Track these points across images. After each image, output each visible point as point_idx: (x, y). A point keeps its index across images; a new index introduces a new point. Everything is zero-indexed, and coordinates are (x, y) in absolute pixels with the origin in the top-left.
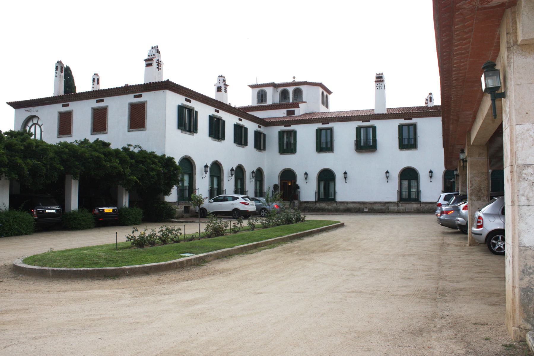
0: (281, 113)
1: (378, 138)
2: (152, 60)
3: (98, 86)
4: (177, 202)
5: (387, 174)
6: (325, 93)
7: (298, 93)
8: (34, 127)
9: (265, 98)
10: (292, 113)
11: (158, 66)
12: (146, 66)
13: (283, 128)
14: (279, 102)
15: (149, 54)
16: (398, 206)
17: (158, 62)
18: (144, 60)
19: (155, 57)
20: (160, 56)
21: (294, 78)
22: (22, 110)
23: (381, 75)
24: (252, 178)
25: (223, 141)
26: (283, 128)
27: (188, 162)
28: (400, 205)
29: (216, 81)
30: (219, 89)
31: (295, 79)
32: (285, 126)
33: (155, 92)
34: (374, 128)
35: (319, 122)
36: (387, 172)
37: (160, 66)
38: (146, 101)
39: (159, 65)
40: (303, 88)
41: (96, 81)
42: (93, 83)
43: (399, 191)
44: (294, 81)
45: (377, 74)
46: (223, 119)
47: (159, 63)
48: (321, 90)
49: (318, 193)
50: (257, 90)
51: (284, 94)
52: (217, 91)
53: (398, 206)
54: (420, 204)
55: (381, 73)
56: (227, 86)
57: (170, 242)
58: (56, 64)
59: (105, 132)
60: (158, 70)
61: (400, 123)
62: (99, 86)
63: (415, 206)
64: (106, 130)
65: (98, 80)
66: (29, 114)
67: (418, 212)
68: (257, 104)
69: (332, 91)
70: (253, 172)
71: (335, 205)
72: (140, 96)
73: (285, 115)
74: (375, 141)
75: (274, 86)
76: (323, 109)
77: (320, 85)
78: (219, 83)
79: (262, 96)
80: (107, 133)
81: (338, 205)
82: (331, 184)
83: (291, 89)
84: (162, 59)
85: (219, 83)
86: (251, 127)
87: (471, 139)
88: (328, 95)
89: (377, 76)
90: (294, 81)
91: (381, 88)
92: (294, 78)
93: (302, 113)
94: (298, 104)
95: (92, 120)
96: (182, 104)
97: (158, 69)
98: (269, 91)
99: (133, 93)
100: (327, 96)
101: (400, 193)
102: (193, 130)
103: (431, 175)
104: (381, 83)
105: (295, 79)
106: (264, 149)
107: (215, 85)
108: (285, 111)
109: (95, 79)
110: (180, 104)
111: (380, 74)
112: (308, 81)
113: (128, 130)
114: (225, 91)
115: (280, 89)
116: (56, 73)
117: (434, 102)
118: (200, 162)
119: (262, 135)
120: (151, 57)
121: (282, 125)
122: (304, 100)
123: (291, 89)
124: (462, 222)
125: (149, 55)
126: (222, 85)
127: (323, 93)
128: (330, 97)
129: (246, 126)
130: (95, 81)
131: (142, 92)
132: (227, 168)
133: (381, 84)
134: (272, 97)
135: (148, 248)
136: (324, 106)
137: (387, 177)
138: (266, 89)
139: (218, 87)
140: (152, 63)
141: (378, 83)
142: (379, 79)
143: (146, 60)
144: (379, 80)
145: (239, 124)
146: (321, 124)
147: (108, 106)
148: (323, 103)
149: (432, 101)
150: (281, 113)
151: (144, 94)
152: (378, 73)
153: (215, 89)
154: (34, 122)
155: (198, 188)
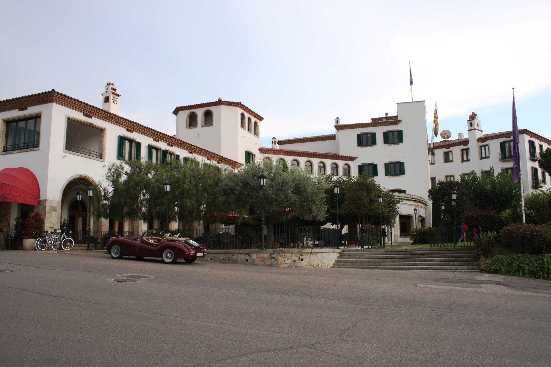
6: (253, 119)
9: (380, 138)
29: (103, 90)
30: (107, 100)
32: (464, 146)
35: (461, 145)
48: (240, 111)
54: (520, 137)
58: (106, 86)
61: (247, 150)
78: (107, 92)
85: (107, 92)
87: (11, 222)
88: (258, 121)
94: (92, 117)
95: (16, 117)
100: (256, 123)
124: (168, 182)
127: (243, 115)
128: (261, 124)
135: (65, 157)
136: (245, 130)
139: (106, 97)
142: (411, 83)
153: (102, 99)
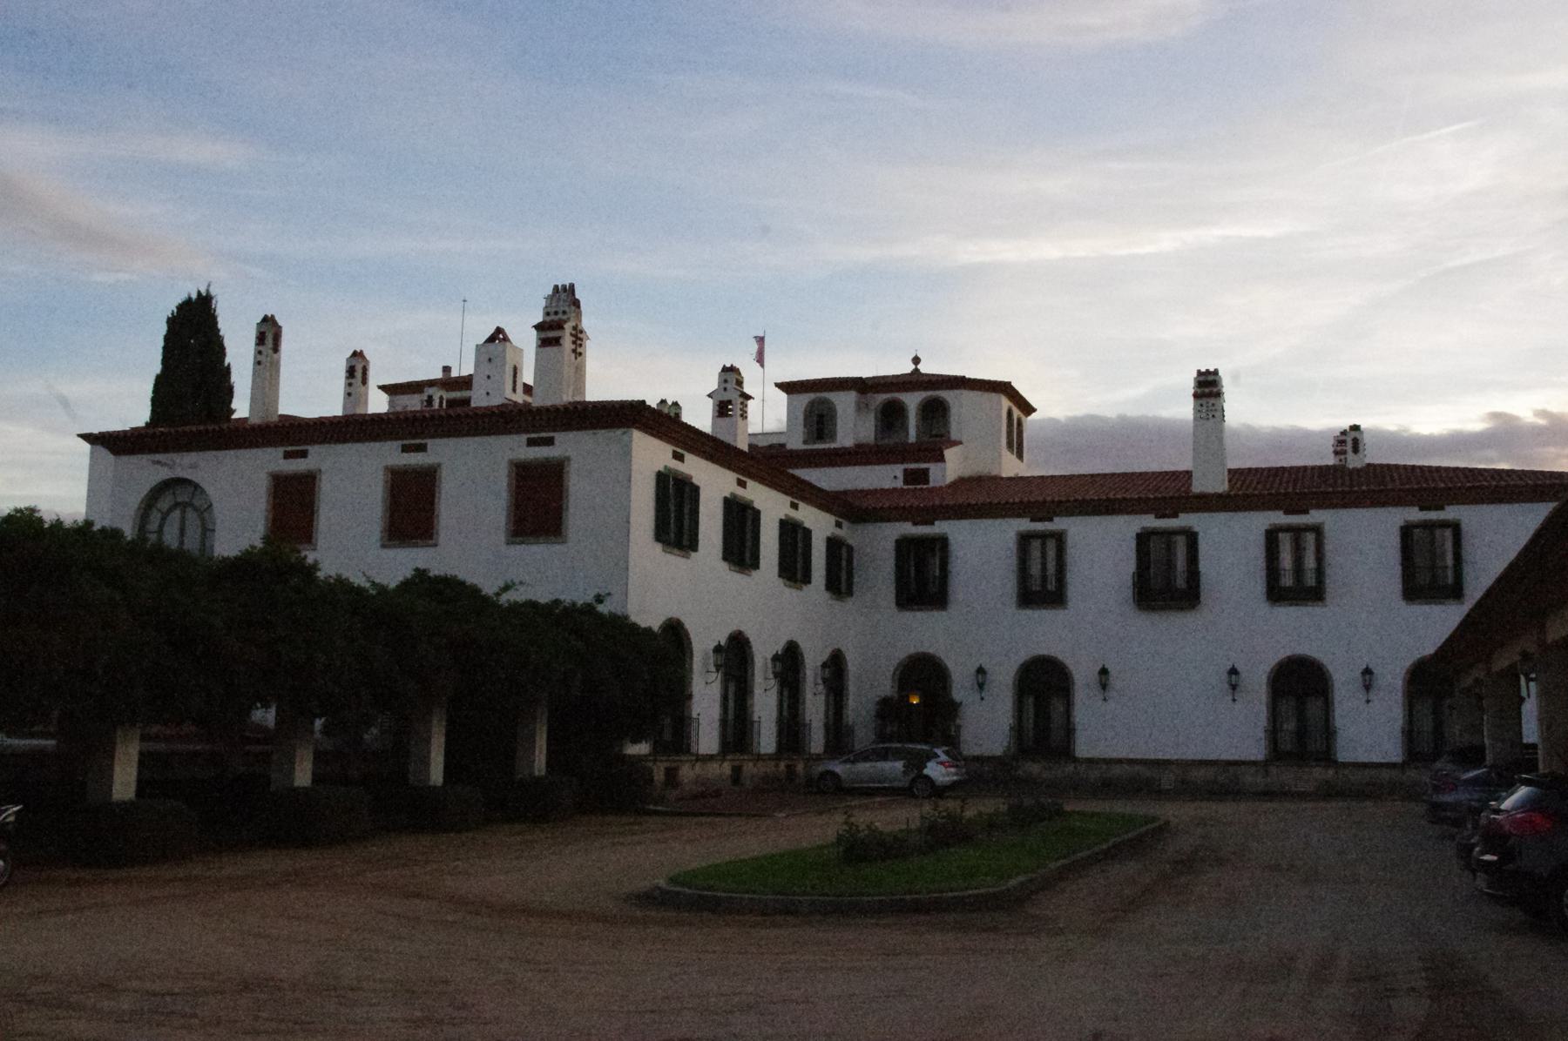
0: (887, 477)
1: (1203, 566)
2: (559, 326)
3: (363, 388)
4: (650, 755)
5: (1234, 676)
6: (1016, 413)
7: (935, 412)
8: (177, 514)
10: (923, 476)
11: (573, 347)
12: (540, 343)
13: (908, 529)
14: (876, 439)
15: (546, 307)
16: (1267, 773)
17: (574, 332)
18: (534, 326)
19: (569, 319)
20: (579, 315)
21: (916, 360)
22: (142, 460)
23: (1211, 378)
24: (713, 669)
25: (755, 573)
26: (908, 529)
27: (675, 631)
28: (1273, 770)
31: (919, 367)
33: (595, 434)
34: (1192, 538)
36: (1233, 671)
37: (581, 345)
38: (568, 459)
39: (579, 342)
40: (959, 402)
41: (359, 374)
42: (351, 381)
43: (1271, 728)
44: (916, 370)
45: (1199, 372)
46: (757, 505)
47: (578, 337)
48: (1006, 403)
49: (1018, 730)
50: (805, 399)
51: (891, 415)
52: (717, 414)
53: (1267, 773)
55: (1212, 369)
56: (748, 397)
57: (1135, 842)
59: (430, 542)
60: (576, 358)
62: (367, 388)
63: (1319, 773)
64: (435, 536)
65: (365, 371)
66: (164, 474)
67: (1328, 793)
68: (805, 442)
69: (1034, 405)
70: (718, 649)
71: (1070, 768)
72: (549, 442)
73: (899, 484)
74: (1194, 575)
75: (861, 386)
76: (1010, 467)
77: (1005, 389)
78: (725, 389)
79: (821, 416)
80: (436, 545)
81: (1082, 768)
82: (1057, 706)
83: (912, 401)
84: (586, 323)
85: (725, 389)
86: (819, 524)
89: (1202, 379)
90: (916, 370)
91: (1213, 416)
92: (916, 360)
93: (951, 476)
96: (666, 467)
97: (573, 355)
98: (844, 402)
99: (527, 431)
100: (1020, 424)
101: (1273, 733)
102: (688, 543)
103: (1367, 683)
104: (1212, 401)
105: (919, 367)
106: (850, 593)
107: (710, 396)
108: (898, 470)
109: (356, 368)
110: (662, 469)
111: (1208, 372)
112: (967, 376)
113: (508, 540)
114: (742, 415)
115: (882, 397)
116: (260, 352)
117: (1366, 453)
118: (704, 640)
119: (844, 551)
120: (553, 317)
121: (906, 520)
122: (954, 436)
123: (912, 401)
125: (549, 310)
126: (732, 395)
127: (1010, 413)
129: (807, 525)
130: (356, 374)
131: (555, 431)
132: (763, 651)
133: (1213, 405)
134: (852, 427)
137: (1234, 687)
138: (833, 396)
140: (560, 337)
141: (1204, 401)
143: (538, 327)
144: (1207, 390)
145: (792, 519)
146: (1029, 519)
147: (439, 465)
148: (1010, 445)
149: (1361, 448)
150: (887, 477)
151: (559, 437)
152: (1203, 370)
154: (180, 499)
155: (699, 715)
